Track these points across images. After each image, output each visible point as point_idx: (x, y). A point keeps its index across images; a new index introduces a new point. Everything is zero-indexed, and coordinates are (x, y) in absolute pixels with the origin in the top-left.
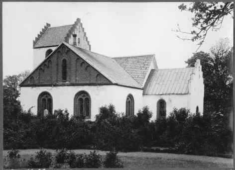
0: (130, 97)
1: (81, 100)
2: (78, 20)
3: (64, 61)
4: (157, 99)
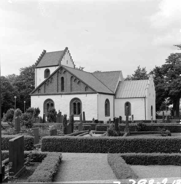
0: (107, 101)
1: (75, 104)
2: (67, 48)
3: (62, 78)
4: (125, 101)
